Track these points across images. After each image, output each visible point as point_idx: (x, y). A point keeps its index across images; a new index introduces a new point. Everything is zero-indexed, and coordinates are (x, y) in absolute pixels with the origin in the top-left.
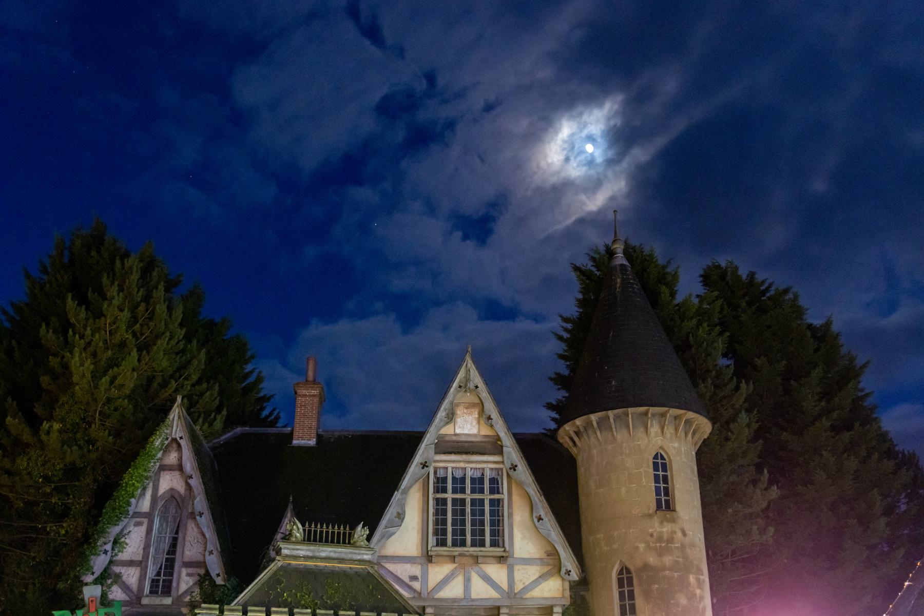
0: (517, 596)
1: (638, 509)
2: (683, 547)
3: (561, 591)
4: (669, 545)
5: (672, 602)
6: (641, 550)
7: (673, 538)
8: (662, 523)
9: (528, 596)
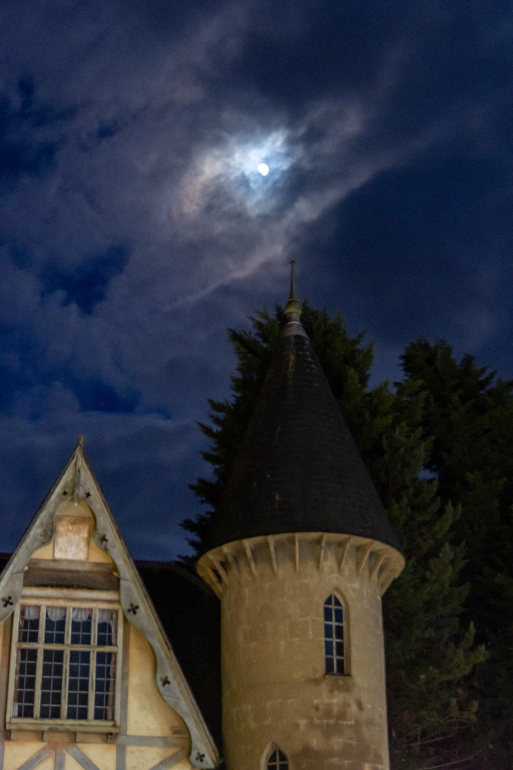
2: (358, 725)
4: (340, 722)
6: (302, 728)
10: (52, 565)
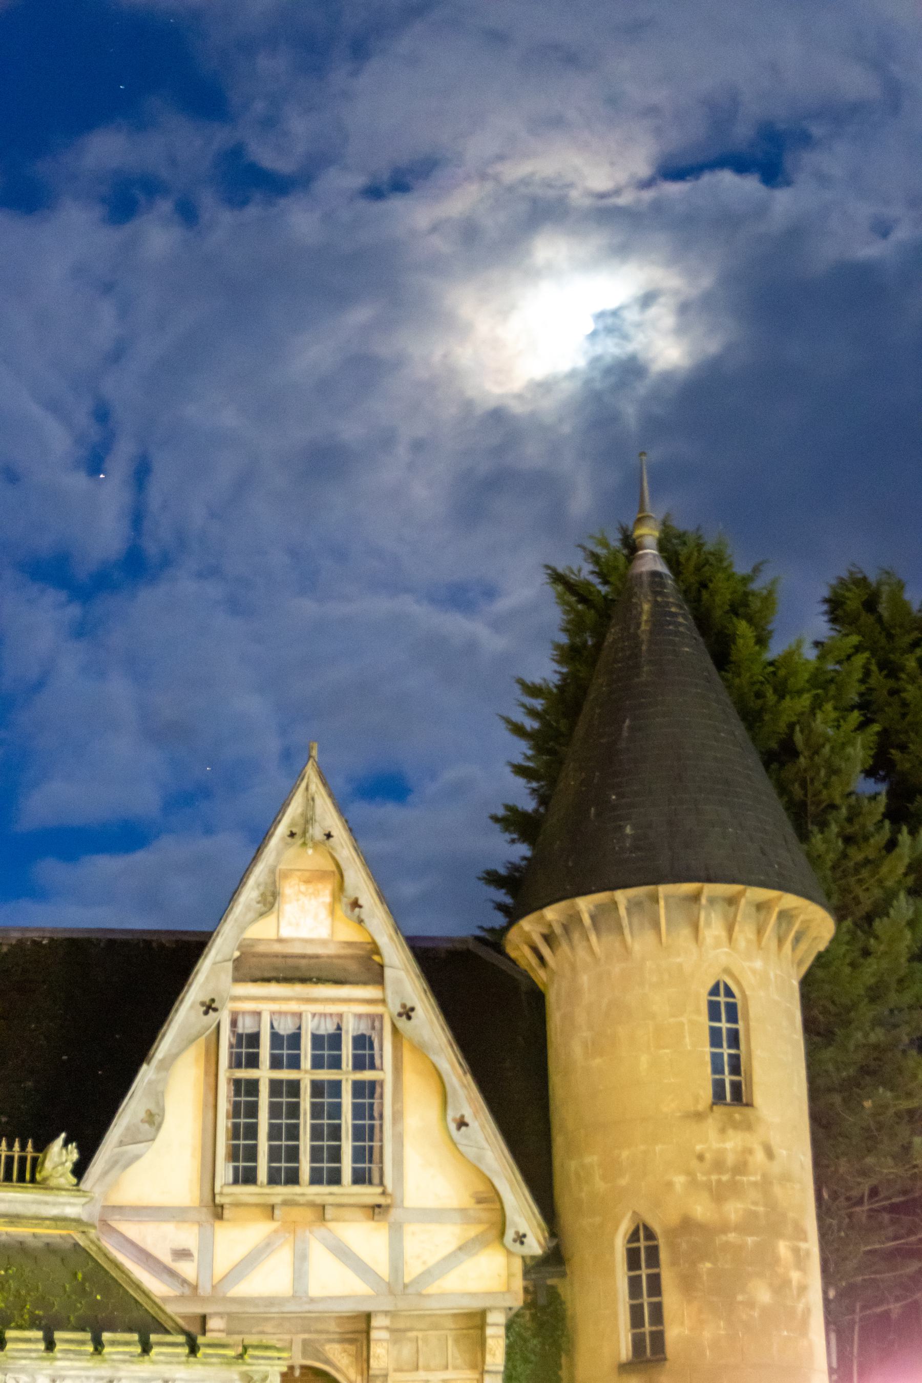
6: (678, 1188)
7: (745, 1164)
8: (723, 1131)
10: (278, 948)
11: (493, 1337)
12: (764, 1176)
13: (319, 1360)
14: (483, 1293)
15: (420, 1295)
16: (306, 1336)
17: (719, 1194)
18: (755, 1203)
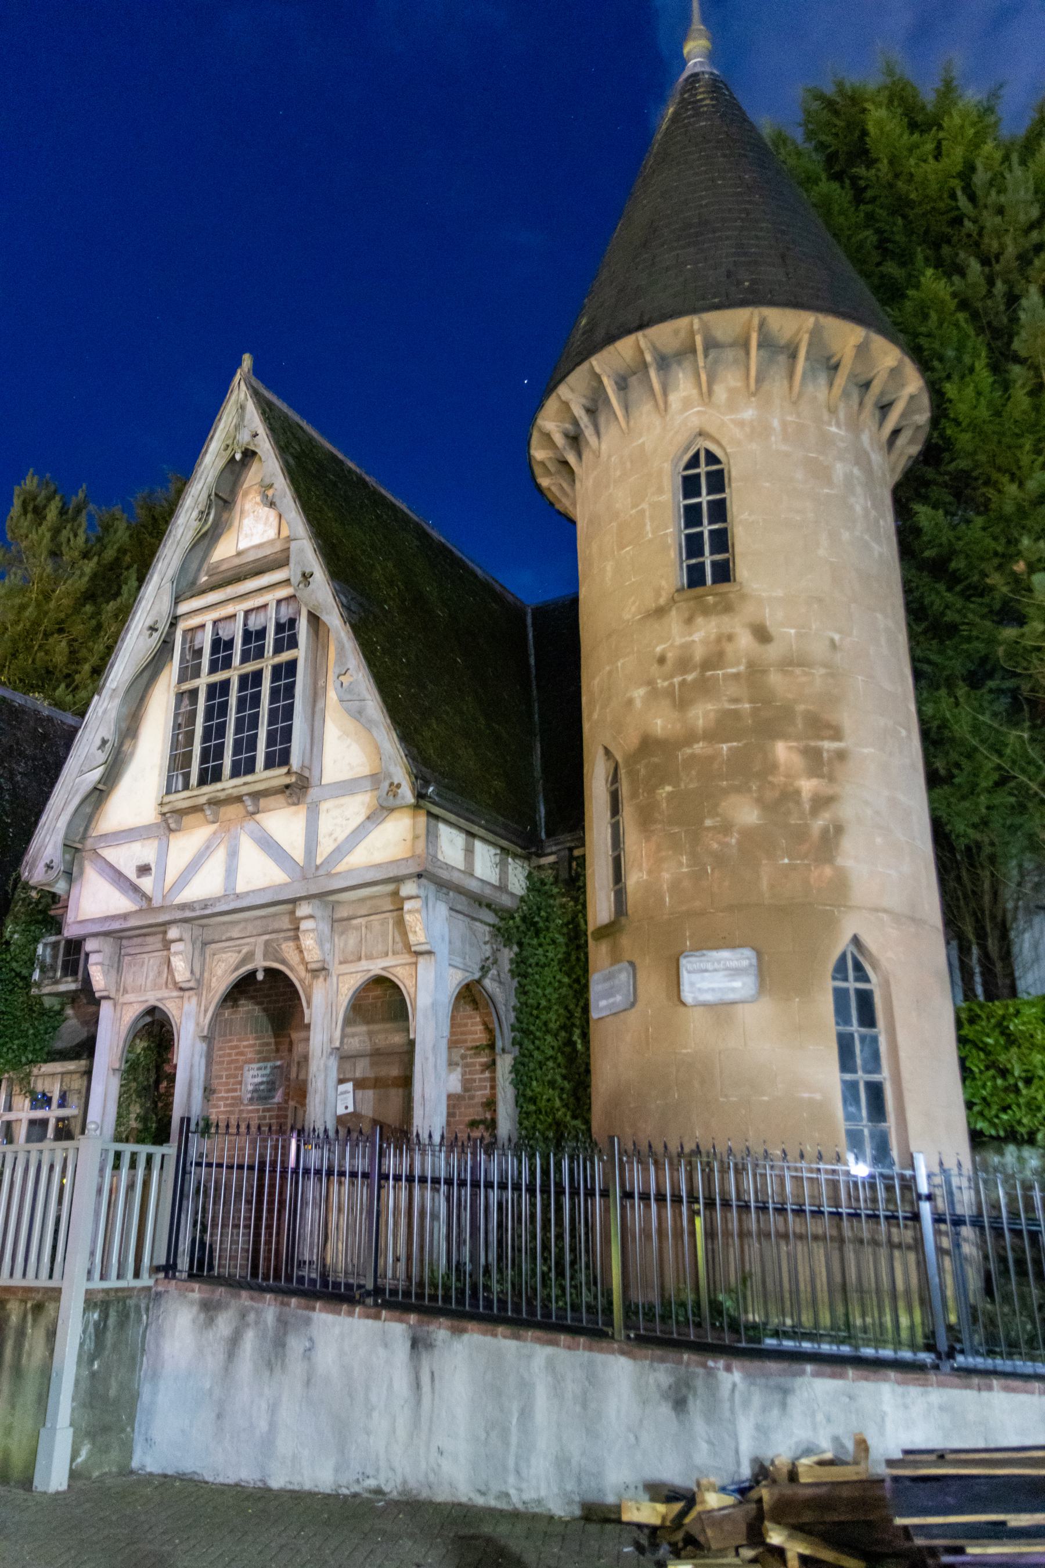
0: (321, 872)
1: (634, 602)
2: (755, 670)
3: (409, 843)
4: (709, 673)
5: (708, 823)
6: (638, 704)
7: (721, 654)
8: (689, 620)
9: (341, 868)
10: (237, 561)
11: (410, 912)
12: (751, 665)
13: (277, 960)
14: (387, 863)
15: (329, 875)
16: (267, 937)
17: (681, 701)
18: (736, 700)
